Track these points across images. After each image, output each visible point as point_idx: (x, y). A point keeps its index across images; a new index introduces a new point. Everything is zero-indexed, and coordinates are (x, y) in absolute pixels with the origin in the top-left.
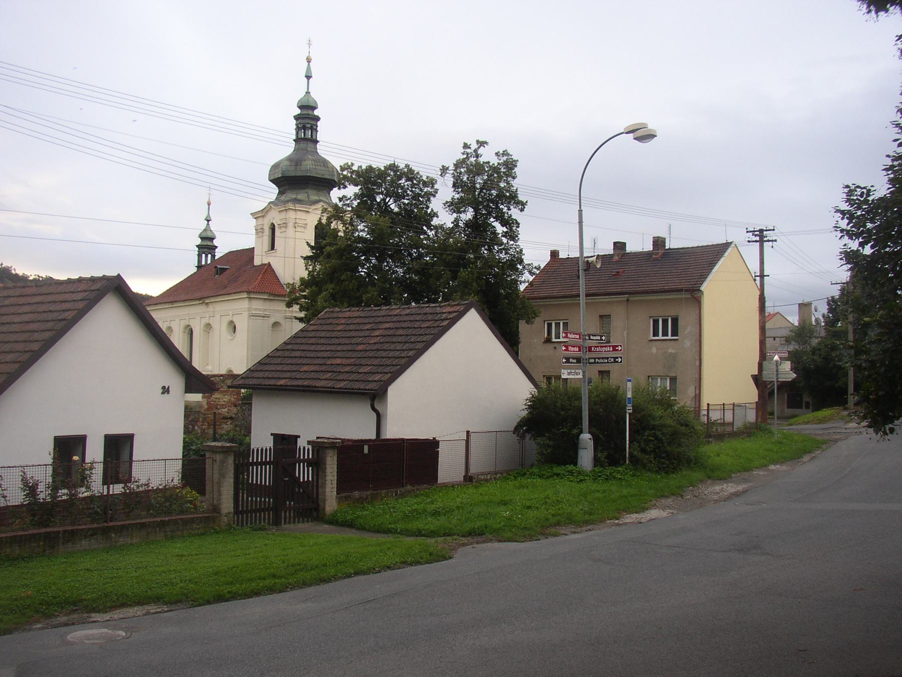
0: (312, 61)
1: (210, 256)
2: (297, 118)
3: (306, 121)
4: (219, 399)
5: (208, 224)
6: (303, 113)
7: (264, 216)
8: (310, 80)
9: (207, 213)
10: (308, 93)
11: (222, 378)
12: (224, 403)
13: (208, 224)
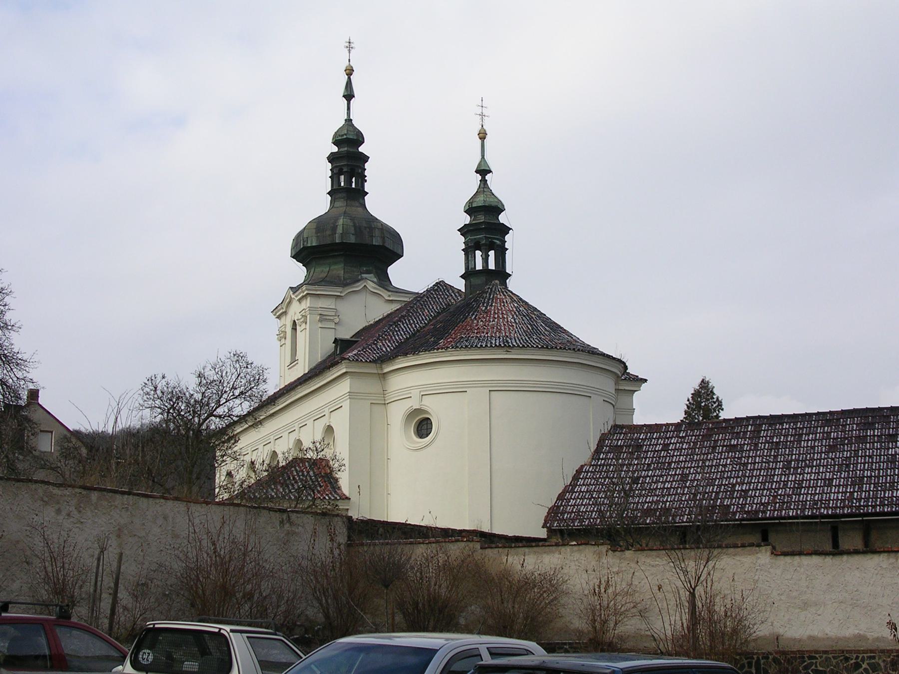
1: (492, 253)
2: (332, 158)
5: (484, 181)
6: (340, 150)
8: (352, 102)
9: (480, 157)
10: (349, 121)
13: (484, 181)
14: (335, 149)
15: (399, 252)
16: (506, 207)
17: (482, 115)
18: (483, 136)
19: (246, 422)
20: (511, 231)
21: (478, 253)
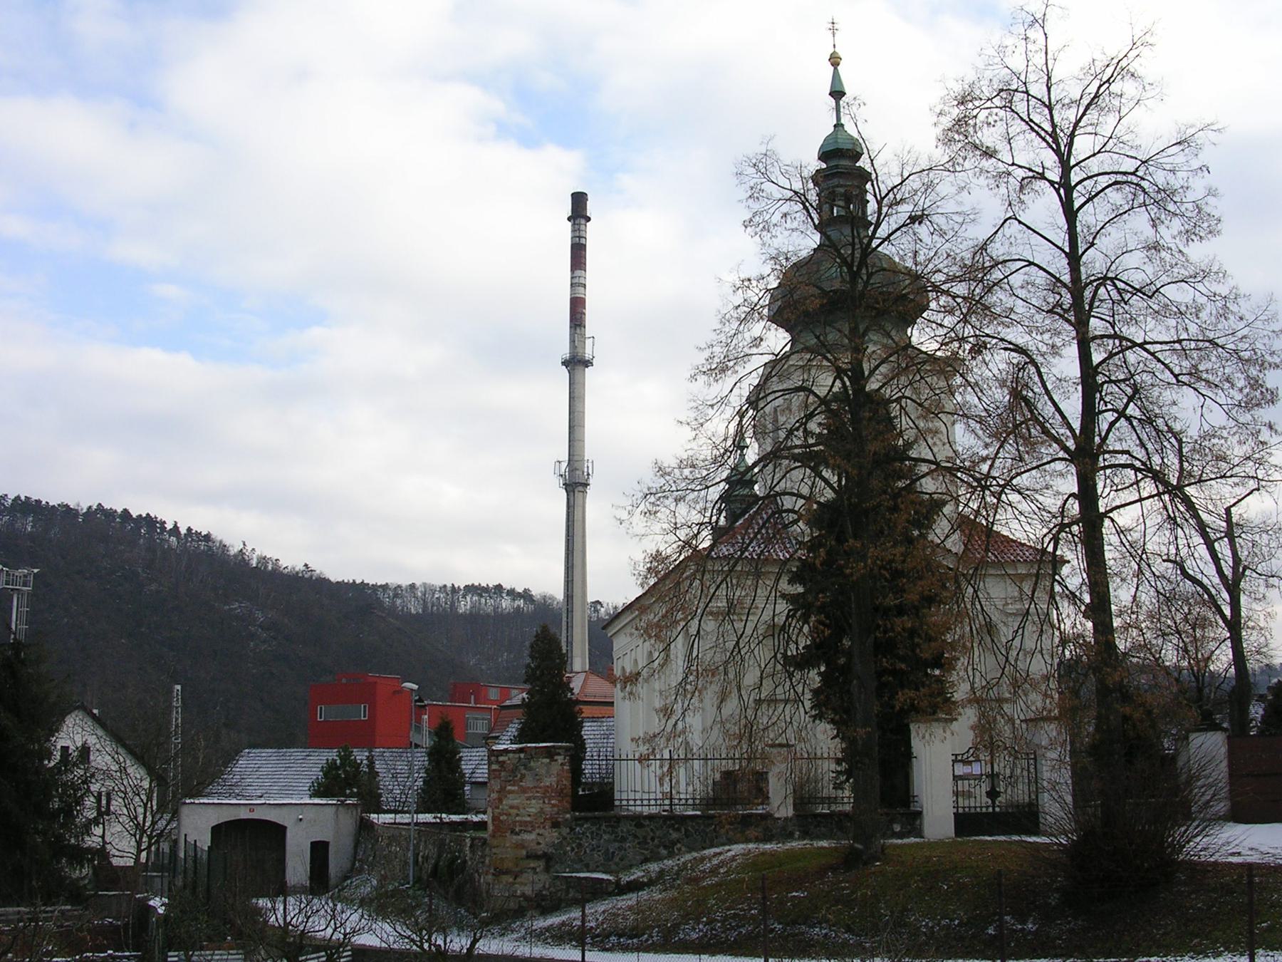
0: (841, 63)
3: (835, 181)
4: (518, 808)
10: (839, 126)
11: (522, 755)
12: (528, 819)
19: (652, 596)
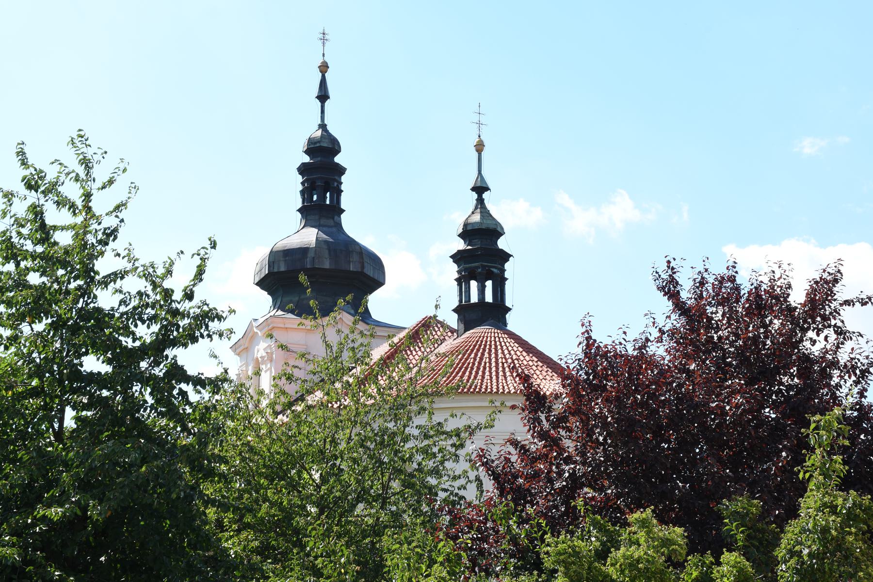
1: (489, 284)
5: (480, 201)
7: (247, 348)
8: (326, 104)
10: (323, 126)
13: (480, 201)
14: (307, 159)
15: (381, 281)
16: (505, 231)
17: (479, 124)
18: (480, 147)
20: (511, 258)
21: (474, 284)
